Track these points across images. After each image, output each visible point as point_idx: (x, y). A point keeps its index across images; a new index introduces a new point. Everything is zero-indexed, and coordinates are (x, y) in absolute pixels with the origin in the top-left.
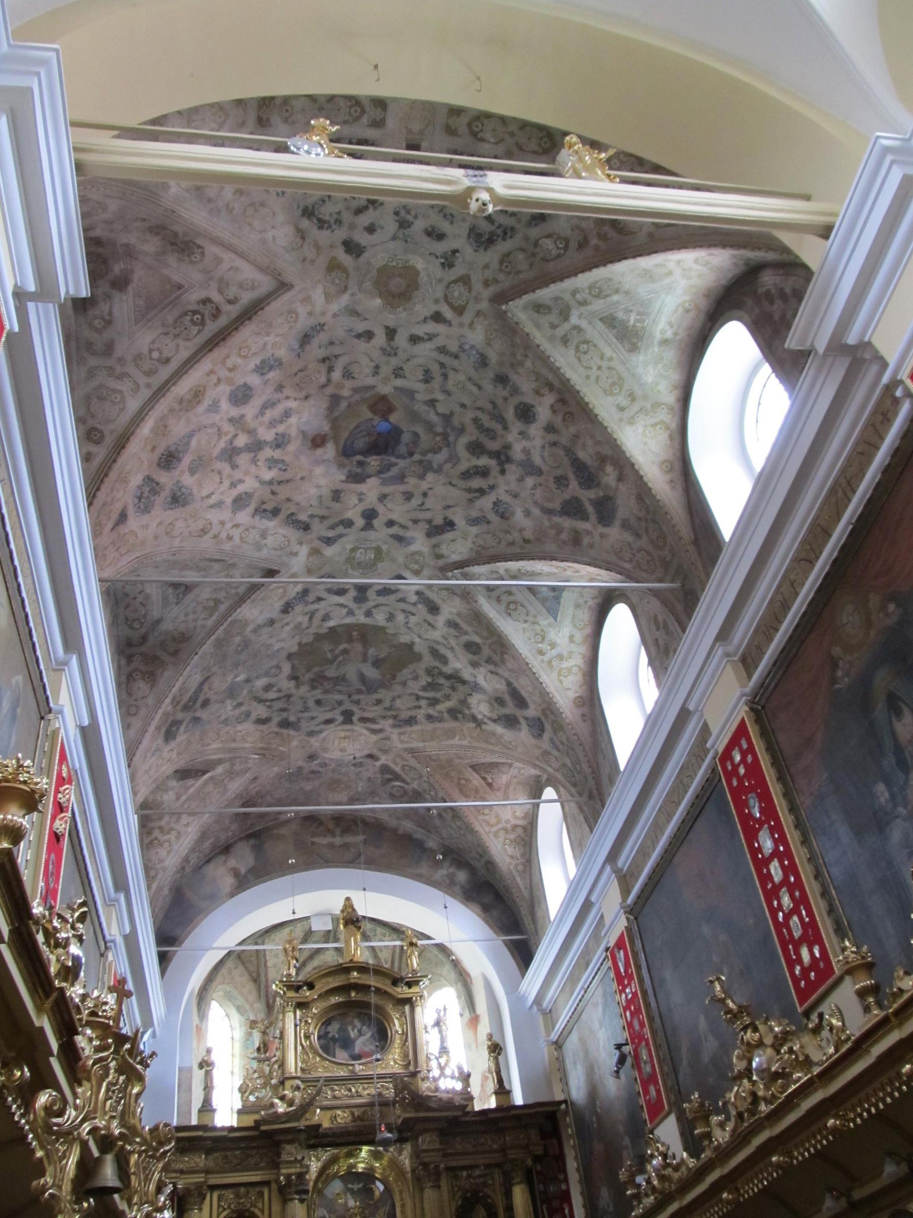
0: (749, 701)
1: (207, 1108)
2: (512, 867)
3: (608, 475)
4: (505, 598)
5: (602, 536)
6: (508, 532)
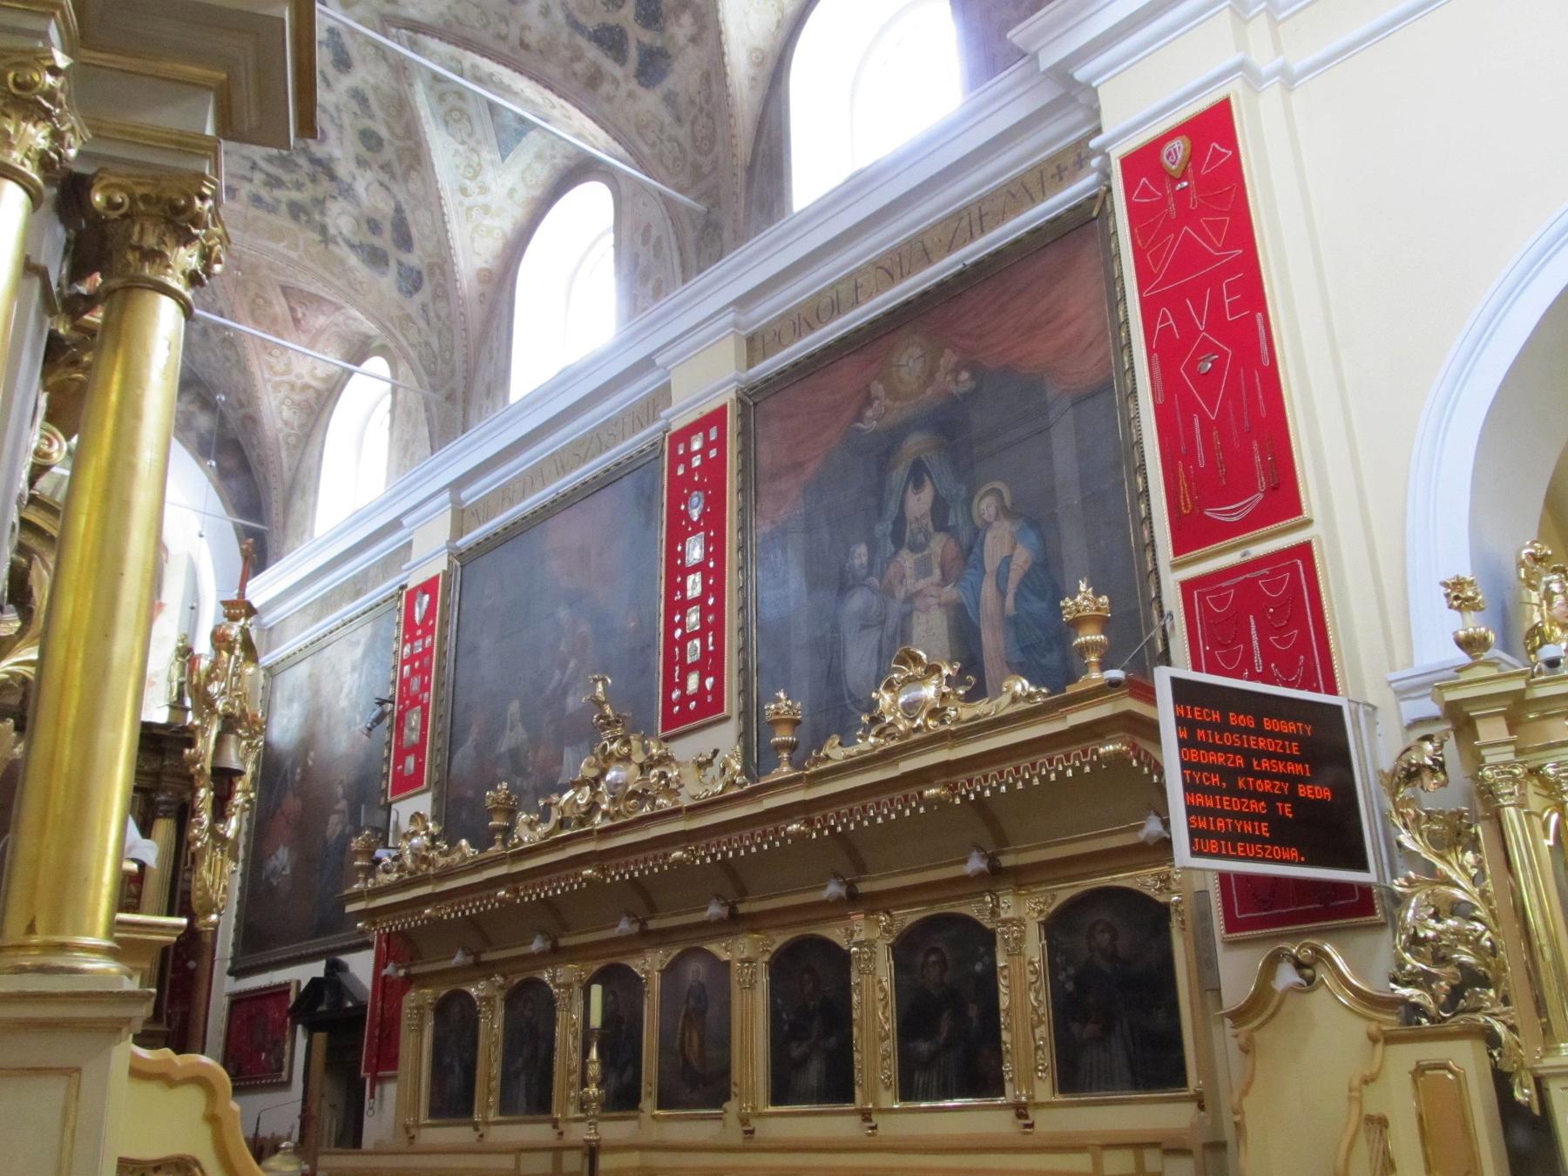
0: (741, 389)
2: (281, 436)
3: (681, 26)
4: (452, 100)
5: (631, 95)
6: (504, 19)
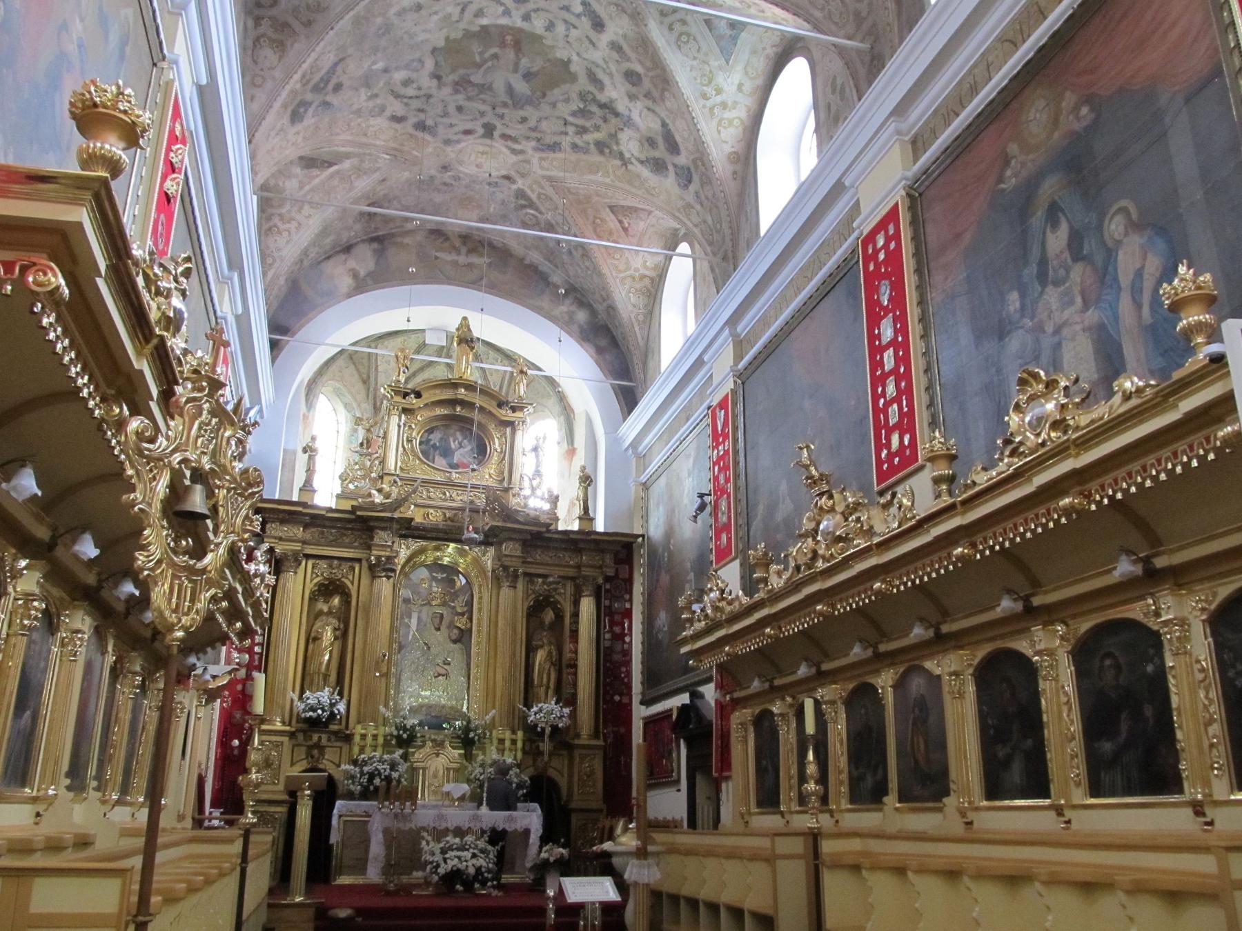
1: (308, 487)
4: (678, 27)
